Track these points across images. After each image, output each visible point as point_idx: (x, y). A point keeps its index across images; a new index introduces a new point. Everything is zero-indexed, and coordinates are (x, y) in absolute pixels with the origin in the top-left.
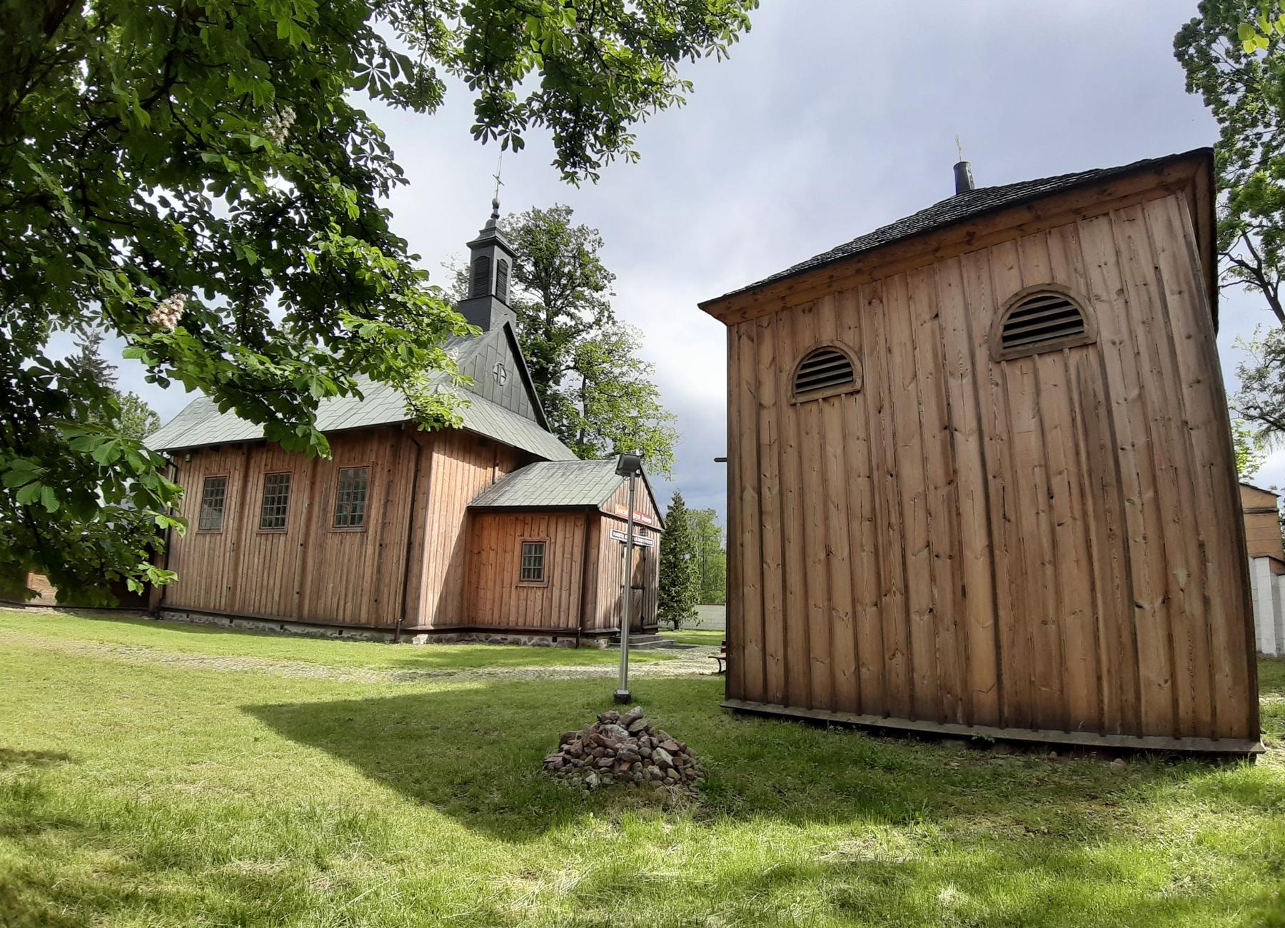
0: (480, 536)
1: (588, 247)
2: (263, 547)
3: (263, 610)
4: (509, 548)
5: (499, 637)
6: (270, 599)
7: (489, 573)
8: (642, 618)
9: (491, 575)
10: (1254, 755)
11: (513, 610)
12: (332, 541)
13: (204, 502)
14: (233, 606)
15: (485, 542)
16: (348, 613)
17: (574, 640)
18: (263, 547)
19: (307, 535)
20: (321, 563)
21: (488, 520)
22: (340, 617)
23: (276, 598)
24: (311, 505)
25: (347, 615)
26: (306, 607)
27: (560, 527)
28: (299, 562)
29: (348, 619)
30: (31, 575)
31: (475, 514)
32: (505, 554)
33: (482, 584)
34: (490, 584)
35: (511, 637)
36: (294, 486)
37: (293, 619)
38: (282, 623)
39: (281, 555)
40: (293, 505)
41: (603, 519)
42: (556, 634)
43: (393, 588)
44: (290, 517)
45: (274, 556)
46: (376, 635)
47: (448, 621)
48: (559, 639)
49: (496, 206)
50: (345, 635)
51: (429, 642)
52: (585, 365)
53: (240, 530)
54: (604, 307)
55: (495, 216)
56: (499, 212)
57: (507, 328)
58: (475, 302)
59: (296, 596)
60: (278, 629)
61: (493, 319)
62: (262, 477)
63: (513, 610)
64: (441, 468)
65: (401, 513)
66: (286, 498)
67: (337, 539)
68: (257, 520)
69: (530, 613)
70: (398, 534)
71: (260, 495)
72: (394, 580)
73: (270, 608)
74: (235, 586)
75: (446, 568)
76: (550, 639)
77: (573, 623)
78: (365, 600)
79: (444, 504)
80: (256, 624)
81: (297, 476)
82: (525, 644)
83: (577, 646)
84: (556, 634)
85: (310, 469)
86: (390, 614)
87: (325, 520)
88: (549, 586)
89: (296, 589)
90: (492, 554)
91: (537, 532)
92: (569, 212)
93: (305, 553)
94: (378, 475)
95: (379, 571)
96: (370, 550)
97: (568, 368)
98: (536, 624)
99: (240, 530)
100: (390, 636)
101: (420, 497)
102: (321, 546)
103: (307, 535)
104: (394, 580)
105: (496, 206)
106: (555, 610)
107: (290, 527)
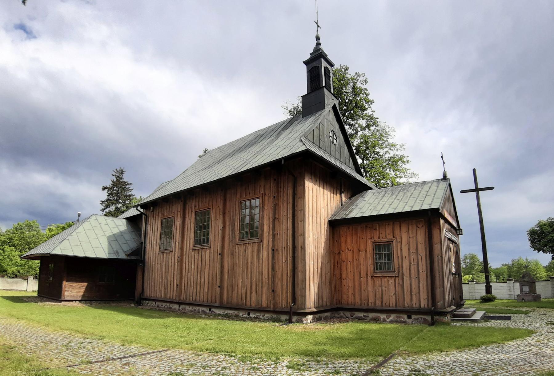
0: (339, 242)
1: (359, 84)
2: (196, 258)
3: (198, 299)
4: (362, 247)
5: (361, 315)
6: (202, 291)
7: (348, 268)
9: (350, 269)
11: (371, 295)
12: (240, 250)
13: (161, 233)
14: (180, 296)
15: (343, 246)
16: (253, 299)
17: (429, 318)
18: (196, 258)
19: (223, 247)
20: (233, 266)
21: (343, 230)
22: (248, 303)
23: (206, 290)
24: (224, 227)
25: (252, 301)
26: (225, 297)
27: (404, 229)
28: (219, 266)
29: (253, 305)
30: (64, 283)
31: (335, 226)
32: (361, 251)
33: (344, 276)
34: (350, 276)
35: (371, 315)
36: (213, 216)
37: (217, 304)
38: (210, 307)
39: (207, 262)
40: (213, 230)
42: (410, 313)
44: (212, 238)
45: (203, 263)
46: (275, 316)
47: (324, 304)
48: (413, 317)
49: (318, 38)
50: (252, 315)
51: (314, 321)
53: (182, 249)
54: (371, 118)
55: (318, 44)
56: (321, 41)
57: (334, 107)
58: (312, 94)
59: (218, 289)
60: (208, 311)
61: (326, 102)
62: (193, 214)
63: (371, 295)
64: (310, 192)
65: (286, 225)
66: (208, 225)
67: (242, 248)
68: (192, 241)
69: (385, 297)
70: (285, 241)
71: (193, 226)
72: (284, 276)
73: (202, 297)
74: (181, 283)
75: (320, 265)
76: (405, 317)
77: (424, 304)
78: (265, 290)
79: (315, 218)
80: (195, 308)
81: (214, 210)
82: (384, 320)
83: (433, 323)
84: (410, 313)
85: (221, 216)
86: (284, 300)
88: (400, 276)
89: (218, 284)
90: (349, 254)
91: (384, 234)
92: (347, 69)
94: (266, 202)
95: (273, 268)
96: (265, 254)
98: (392, 304)
99: (182, 249)
100: (284, 317)
101: (299, 214)
102: (232, 254)
103: (223, 247)
104: (284, 276)
105: (318, 38)
107: (212, 243)
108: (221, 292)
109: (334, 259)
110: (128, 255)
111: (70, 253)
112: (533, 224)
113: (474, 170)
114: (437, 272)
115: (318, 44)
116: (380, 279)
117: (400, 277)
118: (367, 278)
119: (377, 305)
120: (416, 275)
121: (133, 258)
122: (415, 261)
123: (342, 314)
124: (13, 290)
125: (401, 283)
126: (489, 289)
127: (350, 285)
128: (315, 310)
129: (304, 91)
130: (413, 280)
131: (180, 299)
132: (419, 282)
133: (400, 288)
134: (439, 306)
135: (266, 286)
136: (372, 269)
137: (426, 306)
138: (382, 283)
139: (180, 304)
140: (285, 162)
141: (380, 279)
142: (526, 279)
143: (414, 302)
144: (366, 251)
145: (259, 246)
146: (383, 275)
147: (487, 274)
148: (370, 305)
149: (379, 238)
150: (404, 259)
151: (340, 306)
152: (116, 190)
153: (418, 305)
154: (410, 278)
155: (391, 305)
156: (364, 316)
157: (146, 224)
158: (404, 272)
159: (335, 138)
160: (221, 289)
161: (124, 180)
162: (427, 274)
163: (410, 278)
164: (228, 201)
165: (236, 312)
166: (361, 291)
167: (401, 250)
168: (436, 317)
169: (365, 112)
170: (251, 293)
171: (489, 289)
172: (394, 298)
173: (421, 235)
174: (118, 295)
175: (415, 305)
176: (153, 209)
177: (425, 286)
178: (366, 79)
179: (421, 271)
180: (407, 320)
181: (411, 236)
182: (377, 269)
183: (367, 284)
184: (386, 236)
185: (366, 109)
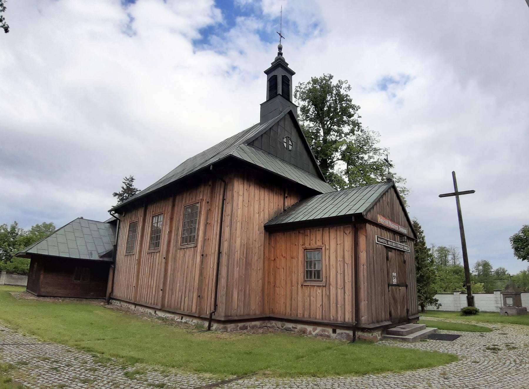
1: (343, 92)
8: (408, 311)
10: (418, 318)
12: (180, 254)
27: (333, 235)
33: (278, 284)
41: (368, 226)
42: (335, 326)
43: (210, 287)
45: (154, 266)
48: (338, 331)
52: (346, 157)
55: (280, 54)
58: (270, 102)
59: (161, 292)
60: (153, 313)
63: (300, 304)
69: (313, 308)
73: (150, 301)
76: (330, 330)
77: (349, 317)
87: (177, 242)
88: (327, 286)
91: (315, 239)
92: (331, 77)
93: (166, 263)
97: (338, 159)
98: (318, 317)
99: (140, 252)
105: (280, 48)
106: (333, 305)
108: (163, 295)
109: (269, 266)
110: (101, 257)
111: (45, 253)
112: (516, 230)
113: (454, 173)
114: (362, 283)
115: (280, 54)
116: (309, 289)
117: (327, 285)
118: (298, 287)
119: (306, 316)
120: (343, 285)
121: (106, 259)
122: (342, 270)
123: (274, 324)
124: (18, 286)
125: (328, 294)
126: (471, 301)
127: (282, 293)
128: (223, 319)
129: (264, 98)
130: (339, 291)
131: (136, 301)
132: (345, 293)
133: (327, 299)
134: (363, 322)
135: (197, 291)
136: (302, 276)
137: (350, 321)
138: (310, 292)
139: (136, 305)
140: (213, 168)
141: (309, 289)
142: (510, 290)
143: (339, 316)
144: (298, 258)
145: (194, 250)
146: (312, 284)
147: (468, 285)
148: (299, 316)
149: (310, 244)
150: (331, 267)
151: (272, 315)
152: (126, 196)
153: (342, 320)
154: (337, 288)
155: (318, 317)
156: (293, 327)
157: (119, 228)
158: (331, 283)
159: (290, 143)
160: (163, 293)
161: (133, 187)
162: (352, 285)
163: (337, 288)
164: (176, 206)
165: (173, 316)
166: (291, 300)
167: (329, 257)
168: (359, 334)
169: (352, 118)
170: (185, 297)
171: (471, 301)
172: (321, 309)
173: (348, 241)
174: (92, 294)
175: (340, 319)
176: (125, 214)
177: (350, 297)
178: (349, 85)
179: (346, 281)
180: (332, 335)
181: (339, 243)
182: (307, 278)
183: (297, 294)
184: (316, 243)
185: (353, 115)
